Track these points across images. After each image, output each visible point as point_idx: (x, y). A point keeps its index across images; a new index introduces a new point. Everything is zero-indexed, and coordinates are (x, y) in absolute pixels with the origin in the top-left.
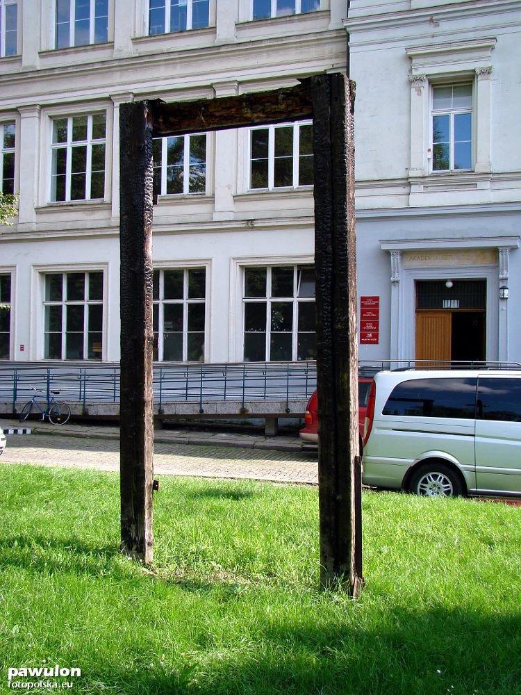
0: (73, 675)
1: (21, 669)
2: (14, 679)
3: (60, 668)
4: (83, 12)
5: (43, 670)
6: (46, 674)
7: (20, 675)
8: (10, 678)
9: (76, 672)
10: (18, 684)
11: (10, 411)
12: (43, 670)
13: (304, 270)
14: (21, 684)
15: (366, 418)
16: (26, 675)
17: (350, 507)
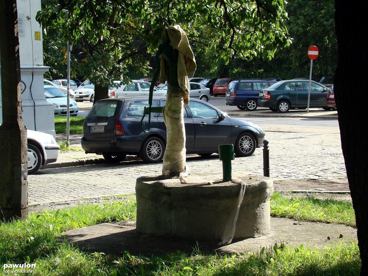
0: (32, 267)
2: (6, 269)
5: (19, 265)
8: (4, 269)
14: (9, 272)
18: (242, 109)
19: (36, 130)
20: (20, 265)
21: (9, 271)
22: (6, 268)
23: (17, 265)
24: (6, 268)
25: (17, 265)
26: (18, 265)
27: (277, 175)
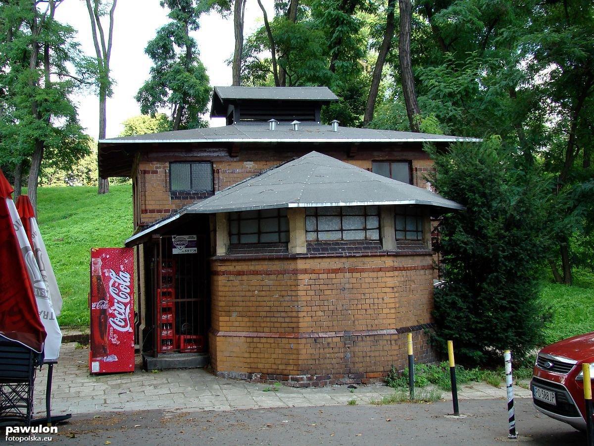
0: (52, 432)
1: (15, 428)
2: (11, 435)
3: (43, 427)
4: (4, 355)
5: (31, 429)
6: (33, 431)
7: (15, 431)
8: (7, 434)
9: (54, 430)
10: (13, 438)
11: (378, 230)
12: (31, 429)
13: (534, 58)
14: (15, 439)
15: (411, 353)
16: (18, 432)
17: (547, 381)
18: (387, 385)
19: (411, 182)
20: (33, 428)
21: (14, 437)
22: (9, 433)
23: (28, 428)
24: (9, 433)
25: (28, 428)
26: (29, 428)
27: (157, 436)
